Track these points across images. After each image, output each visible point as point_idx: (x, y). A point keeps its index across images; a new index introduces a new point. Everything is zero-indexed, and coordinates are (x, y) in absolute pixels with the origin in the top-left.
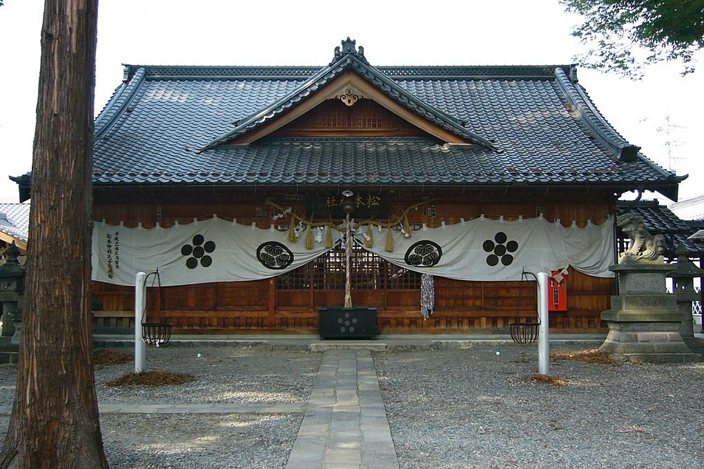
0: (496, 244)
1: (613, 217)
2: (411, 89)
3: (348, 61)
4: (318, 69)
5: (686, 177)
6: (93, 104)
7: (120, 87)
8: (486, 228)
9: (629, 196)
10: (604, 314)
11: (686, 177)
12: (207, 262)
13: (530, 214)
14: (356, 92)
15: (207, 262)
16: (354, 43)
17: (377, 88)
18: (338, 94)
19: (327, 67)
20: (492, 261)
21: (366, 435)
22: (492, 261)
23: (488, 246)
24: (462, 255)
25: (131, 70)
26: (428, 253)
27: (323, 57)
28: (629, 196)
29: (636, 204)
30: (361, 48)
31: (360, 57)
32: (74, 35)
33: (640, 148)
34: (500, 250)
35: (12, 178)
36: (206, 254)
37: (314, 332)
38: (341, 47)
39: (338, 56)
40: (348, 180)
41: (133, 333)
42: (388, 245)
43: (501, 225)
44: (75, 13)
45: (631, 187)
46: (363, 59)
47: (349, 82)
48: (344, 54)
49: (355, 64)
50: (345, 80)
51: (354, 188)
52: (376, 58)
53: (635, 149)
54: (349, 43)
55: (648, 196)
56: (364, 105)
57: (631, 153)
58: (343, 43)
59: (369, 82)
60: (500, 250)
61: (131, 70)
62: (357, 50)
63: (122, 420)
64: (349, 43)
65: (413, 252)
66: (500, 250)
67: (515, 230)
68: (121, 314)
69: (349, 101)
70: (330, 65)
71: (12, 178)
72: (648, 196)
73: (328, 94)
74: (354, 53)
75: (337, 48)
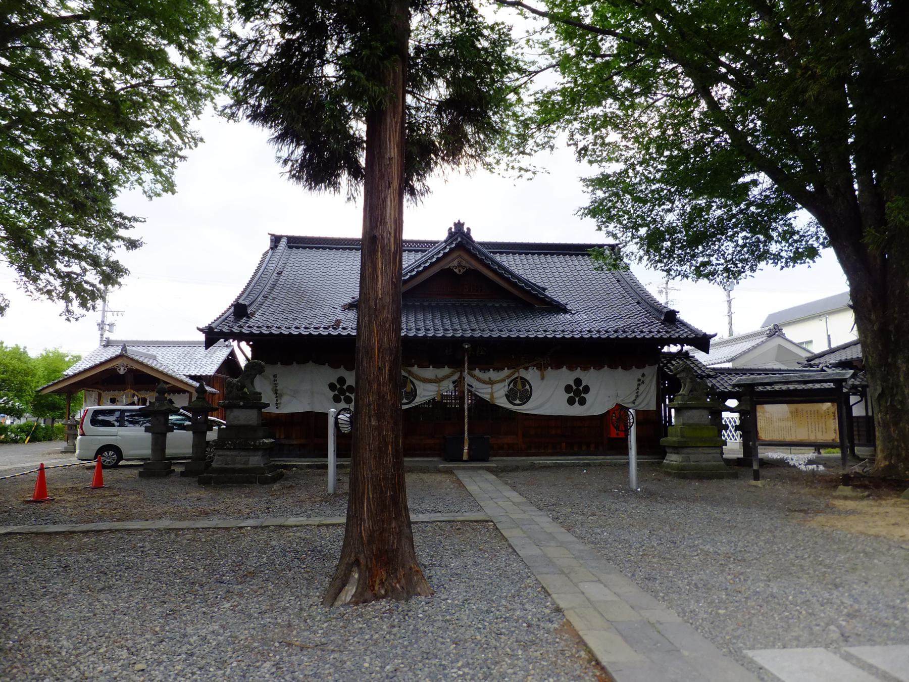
2: (509, 261)
3: (459, 239)
4: (435, 243)
7: (267, 252)
8: (567, 376)
9: (666, 349)
10: (88, 481)
12: (583, 402)
13: (599, 366)
14: (464, 263)
15: (583, 402)
16: (463, 224)
17: (481, 261)
18: (451, 265)
20: (571, 402)
22: (571, 402)
23: (568, 389)
24: (548, 397)
25: (276, 240)
26: (520, 392)
27: (440, 235)
30: (469, 229)
31: (467, 236)
34: (578, 392)
35: (199, 329)
36: (572, 394)
37: (439, 455)
39: (452, 235)
40: (468, 334)
41: (326, 456)
42: (493, 388)
43: (578, 373)
45: (675, 342)
46: (470, 238)
47: (459, 256)
48: (456, 233)
49: (464, 242)
51: (472, 340)
52: (478, 236)
53: (674, 313)
54: (459, 225)
55: (686, 348)
56: (471, 273)
57: (671, 317)
58: (455, 224)
59: (474, 257)
60: (577, 393)
61: (276, 240)
62: (465, 230)
64: (459, 225)
66: (578, 392)
67: (589, 377)
70: (445, 241)
71: (199, 329)
73: (443, 265)
74: (463, 233)
75: (450, 229)
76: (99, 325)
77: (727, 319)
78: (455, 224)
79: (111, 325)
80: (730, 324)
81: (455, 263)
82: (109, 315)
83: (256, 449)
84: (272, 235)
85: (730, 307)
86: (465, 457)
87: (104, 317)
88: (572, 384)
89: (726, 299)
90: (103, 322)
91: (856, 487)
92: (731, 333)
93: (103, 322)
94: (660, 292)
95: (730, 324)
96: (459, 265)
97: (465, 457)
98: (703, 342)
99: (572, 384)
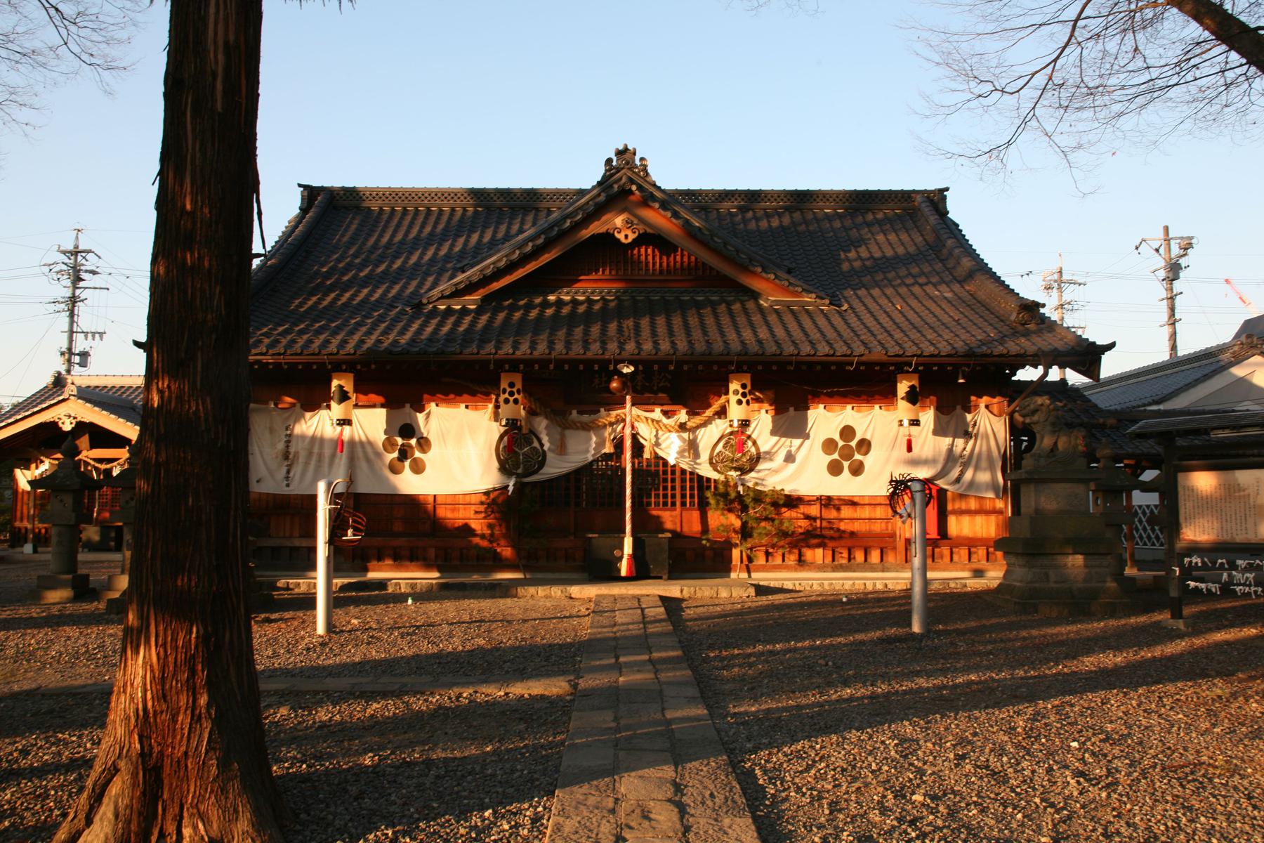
0: (841, 443)
1: (796, 551)
5: (1111, 346)
6: (166, 111)
9: (1028, 374)
11: (1111, 346)
12: (857, 470)
15: (857, 470)
19: (594, 187)
20: (835, 469)
21: (652, 676)
22: (835, 469)
28: (1028, 374)
29: (1041, 386)
32: (219, 86)
33: (1044, 306)
34: (847, 454)
36: (836, 456)
38: (615, 159)
44: (221, 49)
55: (1054, 374)
62: (638, 162)
63: (673, 648)
65: (720, 447)
68: (297, 543)
69: (626, 237)
72: (1054, 374)
75: (609, 161)
76: (63, 354)
77: (1167, 331)
78: (620, 153)
79: (84, 355)
80: (1173, 336)
82: (79, 338)
84: (306, 187)
85: (1172, 309)
87: (71, 341)
88: (837, 437)
89: (1164, 294)
90: (70, 349)
91: (1226, 674)
92: (1174, 348)
93: (70, 349)
94: (1048, 288)
95: (1173, 336)
97: (623, 573)
98: (1087, 355)
99: (837, 437)
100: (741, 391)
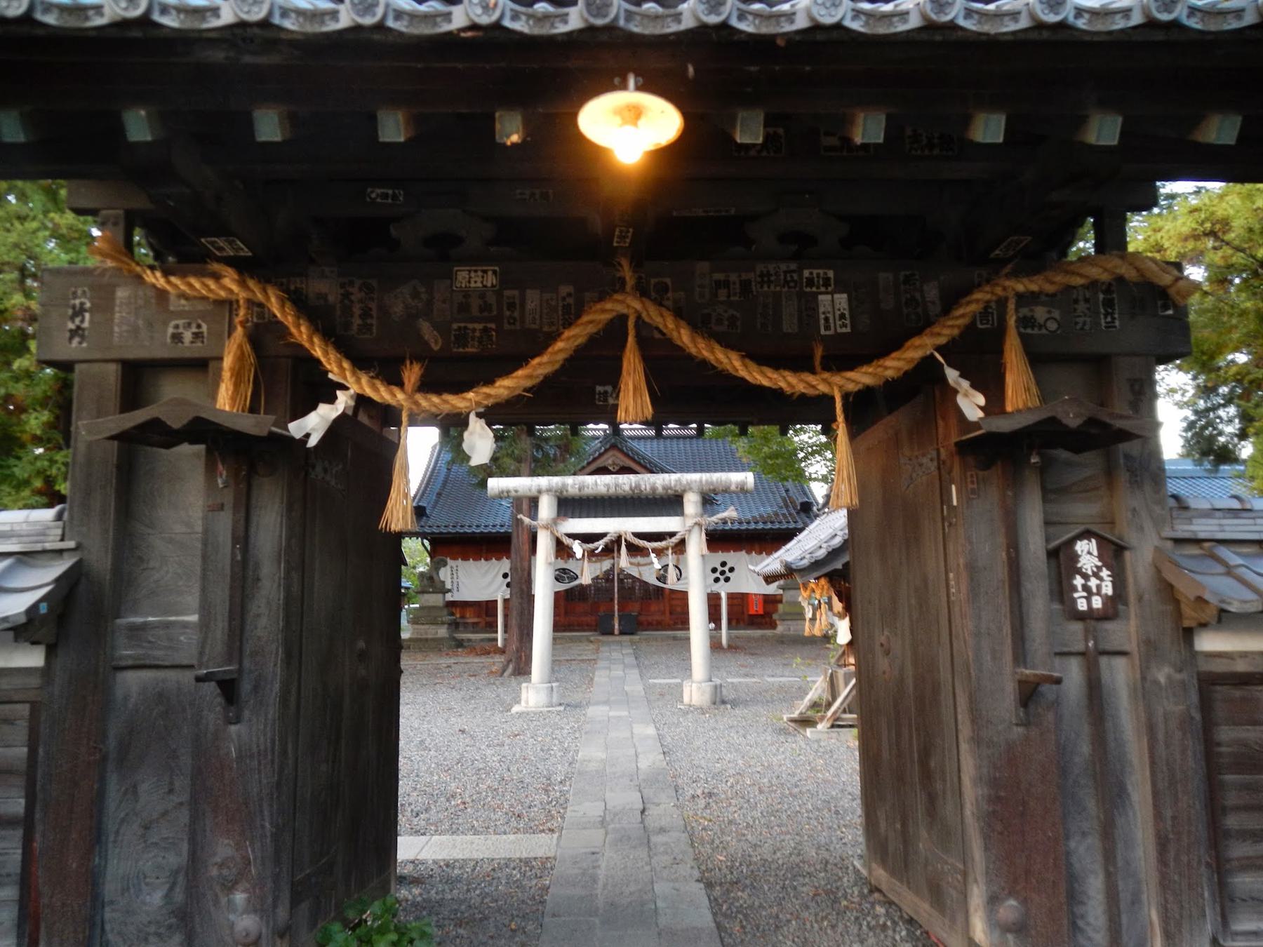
18: (606, 464)
50: (610, 453)
81: (610, 462)
83: (443, 623)
86: (616, 632)
96: (614, 464)
97: (616, 632)
100: (720, 569)
